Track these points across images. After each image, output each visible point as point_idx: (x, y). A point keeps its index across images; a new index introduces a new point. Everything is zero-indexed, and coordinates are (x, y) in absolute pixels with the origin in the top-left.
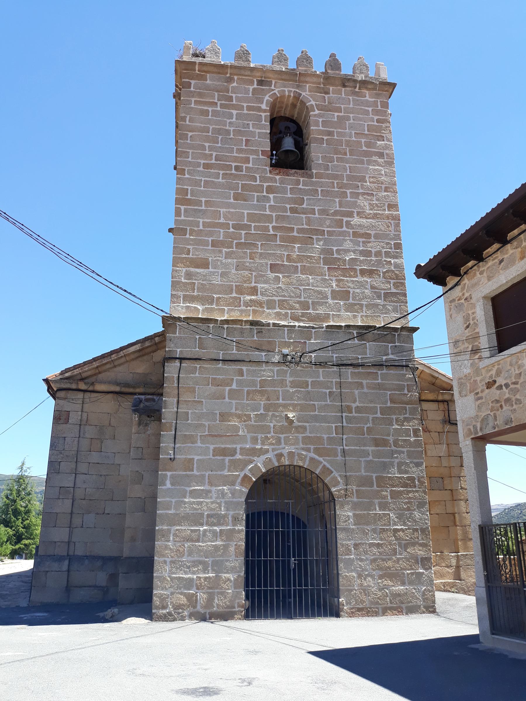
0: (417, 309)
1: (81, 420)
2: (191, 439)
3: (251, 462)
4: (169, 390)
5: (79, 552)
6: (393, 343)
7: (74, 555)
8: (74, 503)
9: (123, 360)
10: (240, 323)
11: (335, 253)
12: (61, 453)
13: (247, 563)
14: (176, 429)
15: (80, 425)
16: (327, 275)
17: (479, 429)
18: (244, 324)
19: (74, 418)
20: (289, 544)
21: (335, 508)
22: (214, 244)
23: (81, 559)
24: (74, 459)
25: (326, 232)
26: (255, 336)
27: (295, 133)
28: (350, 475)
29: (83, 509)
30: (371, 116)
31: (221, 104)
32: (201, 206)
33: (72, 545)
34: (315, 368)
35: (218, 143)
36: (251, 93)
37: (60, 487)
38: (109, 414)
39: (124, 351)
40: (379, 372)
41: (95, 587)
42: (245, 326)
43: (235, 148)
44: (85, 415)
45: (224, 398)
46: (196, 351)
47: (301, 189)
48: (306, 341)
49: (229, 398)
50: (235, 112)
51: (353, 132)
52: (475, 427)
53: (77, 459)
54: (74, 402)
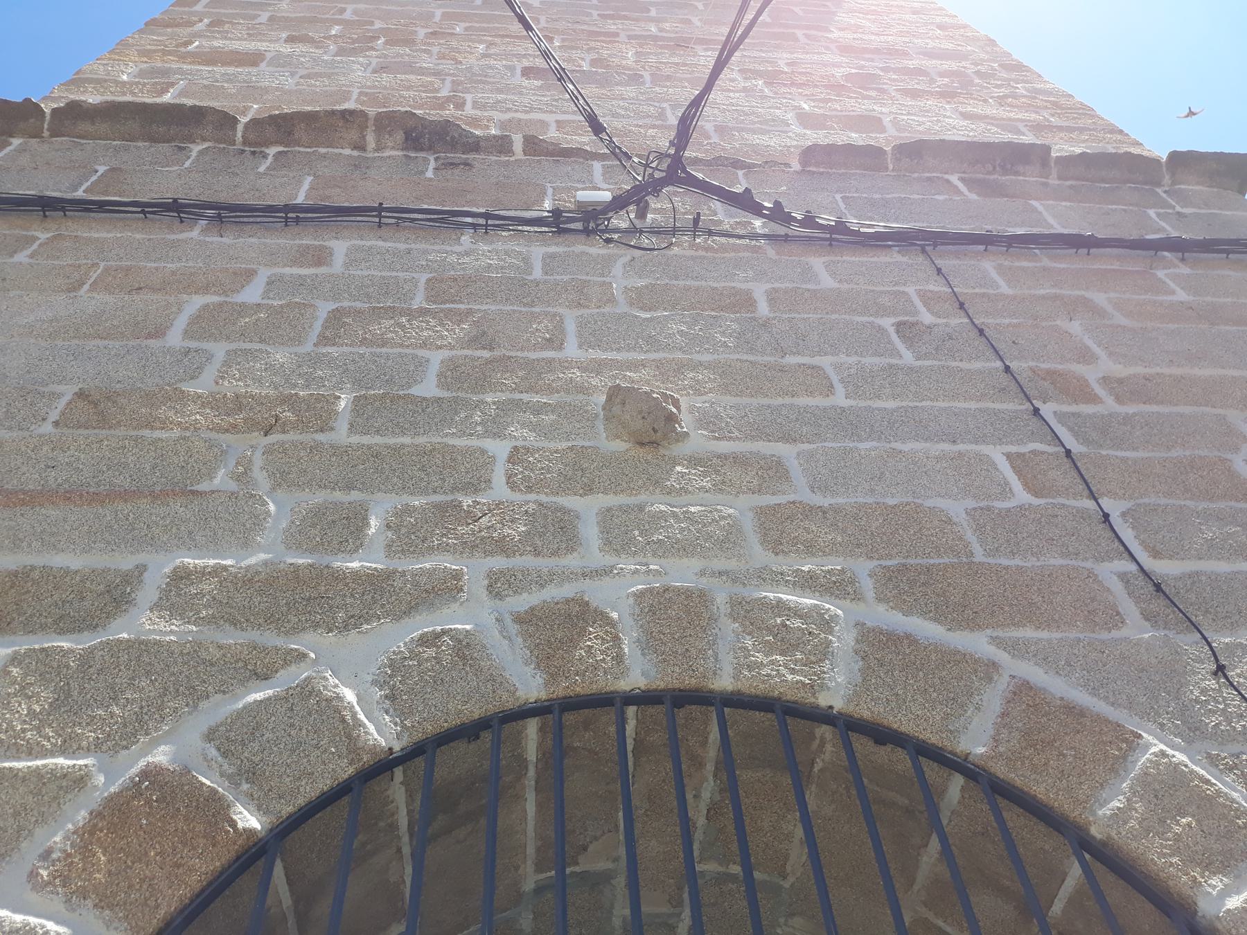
10: (353, 135)
18: (371, 140)
42: (377, 150)
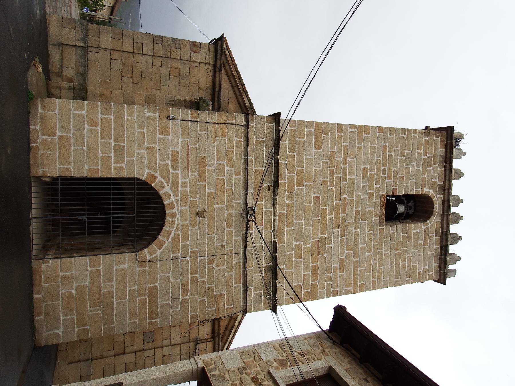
0: (307, 309)
1: (193, 61)
2: (185, 133)
3: (168, 183)
4: (223, 116)
5: (92, 56)
6: (263, 294)
7: (88, 51)
8: (130, 54)
9: (238, 94)
11: (329, 245)
12: (169, 45)
13: (83, 179)
14: (193, 121)
15: (190, 61)
16: (313, 240)
17: (214, 373)
19: (195, 57)
20: (99, 214)
21: (130, 252)
22: (332, 153)
23: (85, 56)
24: (164, 55)
25: (343, 238)
26: (267, 185)
27: (407, 213)
28: (157, 264)
29: (125, 60)
30: (423, 268)
31: (425, 159)
32: (358, 144)
33: (97, 50)
34: (243, 233)
35: (400, 156)
36: (434, 180)
37: (142, 44)
38: (198, 83)
39: (244, 94)
40: (241, 285)
41: (62, 66)
43: (398, 169)
44: (197, 65)
45: (217, 160)
46: (253, 139)
47: (372, 218)
48: (263, 226)
49: (217, 165)
50: (421, 169)
51: (411, 255)
52: (214, 369)
53: (164, 57)
54: (207, 57)
